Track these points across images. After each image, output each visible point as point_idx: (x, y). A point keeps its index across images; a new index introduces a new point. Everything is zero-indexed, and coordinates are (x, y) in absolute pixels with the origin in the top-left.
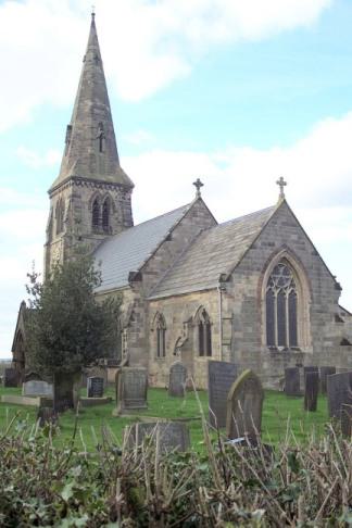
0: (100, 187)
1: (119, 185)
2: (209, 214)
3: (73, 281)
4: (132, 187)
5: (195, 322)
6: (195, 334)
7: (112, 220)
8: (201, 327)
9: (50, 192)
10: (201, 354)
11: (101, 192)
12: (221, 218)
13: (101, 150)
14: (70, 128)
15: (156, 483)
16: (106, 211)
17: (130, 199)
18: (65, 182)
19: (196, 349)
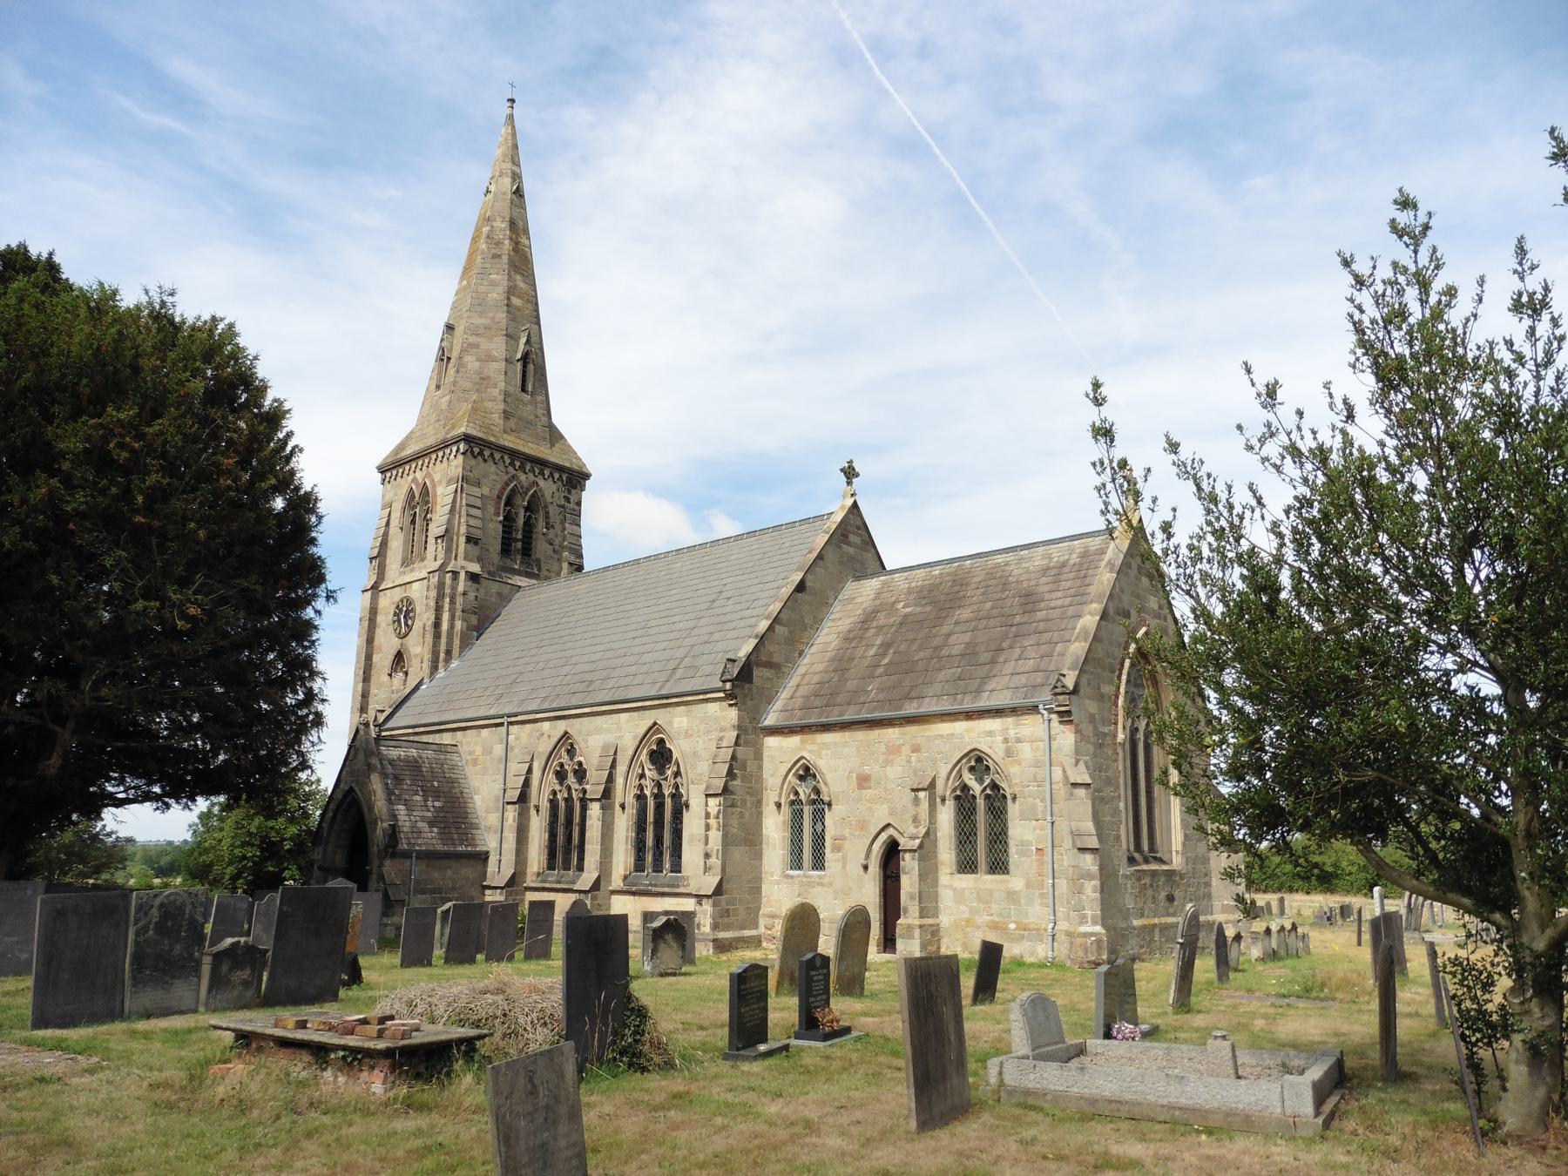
0: (522, 468)
1: (560, 469)
2: (869, 543)
3: (1555, 852)
4: (587, 476)
5: (944, 788)
6: (946, 816)
7: (541, 548)
8: (964, 800)
9: (383, 470)
10: (967, 865)
11: (523, 477)
12: (893, 557)
13: (524, 389)
14: (450, 328)
15: (194, 1037)
16: (529, 527)
17: (579, 504)
18: (444, 445)
19: (946, 853)
